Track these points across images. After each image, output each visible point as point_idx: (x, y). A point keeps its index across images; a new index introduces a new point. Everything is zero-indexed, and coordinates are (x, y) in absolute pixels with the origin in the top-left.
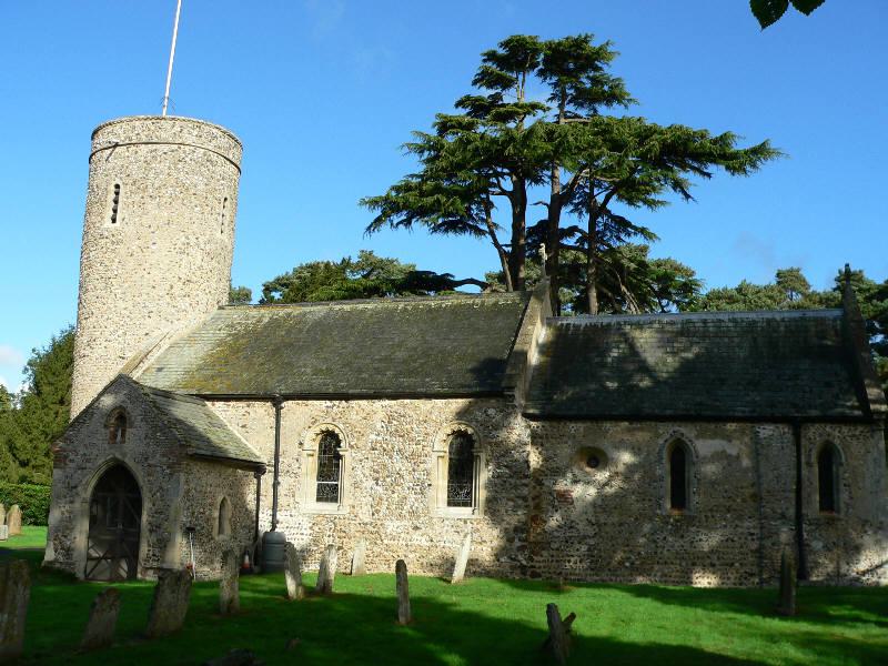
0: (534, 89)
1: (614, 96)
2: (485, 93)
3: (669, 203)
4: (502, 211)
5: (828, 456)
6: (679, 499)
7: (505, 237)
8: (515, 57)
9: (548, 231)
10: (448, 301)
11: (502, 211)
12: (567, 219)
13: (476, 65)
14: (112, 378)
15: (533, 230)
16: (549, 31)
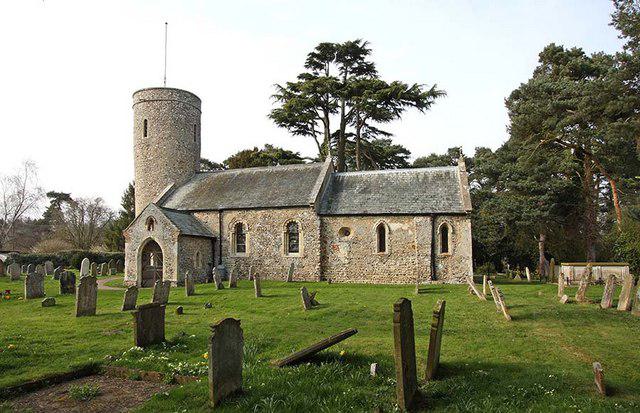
0: (334, 69)
1: (370, 69)
2: (310, 71)
3: (445, 94)
4: (320, 126)
5: (444, 230)
6: (382, 248)
7: (321, 139)
8: (326, 52)
9: (340, 134)
10: (300, 167)
11: (320, 126)
12: (350, 129)
13: (304, 58)
14: (494, 360)
15: (334, 135)
16: (340, 38)
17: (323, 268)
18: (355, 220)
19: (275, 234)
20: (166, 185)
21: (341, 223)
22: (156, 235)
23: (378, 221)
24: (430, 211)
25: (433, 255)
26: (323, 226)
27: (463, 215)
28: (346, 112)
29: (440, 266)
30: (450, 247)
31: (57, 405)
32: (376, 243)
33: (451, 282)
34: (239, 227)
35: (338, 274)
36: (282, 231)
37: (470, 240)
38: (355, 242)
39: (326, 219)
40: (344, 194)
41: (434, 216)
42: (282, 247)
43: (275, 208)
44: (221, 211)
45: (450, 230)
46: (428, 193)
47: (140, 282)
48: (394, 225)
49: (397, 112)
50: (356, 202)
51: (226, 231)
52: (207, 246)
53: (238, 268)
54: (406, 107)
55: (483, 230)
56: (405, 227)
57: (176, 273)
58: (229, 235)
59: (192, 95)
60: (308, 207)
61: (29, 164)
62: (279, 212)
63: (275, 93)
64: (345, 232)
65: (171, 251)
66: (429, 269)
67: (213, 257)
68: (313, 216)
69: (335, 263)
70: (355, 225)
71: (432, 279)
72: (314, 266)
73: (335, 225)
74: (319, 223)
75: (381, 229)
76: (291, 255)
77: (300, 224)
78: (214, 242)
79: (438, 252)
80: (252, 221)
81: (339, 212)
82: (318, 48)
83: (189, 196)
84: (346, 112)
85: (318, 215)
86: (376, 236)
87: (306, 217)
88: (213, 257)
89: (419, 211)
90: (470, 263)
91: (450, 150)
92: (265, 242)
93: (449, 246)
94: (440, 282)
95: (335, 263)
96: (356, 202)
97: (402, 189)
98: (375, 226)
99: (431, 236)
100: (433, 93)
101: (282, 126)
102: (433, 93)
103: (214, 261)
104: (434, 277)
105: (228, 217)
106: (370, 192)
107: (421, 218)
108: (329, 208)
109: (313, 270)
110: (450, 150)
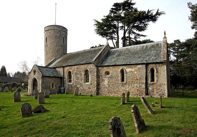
5: (152, 71)
6: (123, 80)
17: (98, 89)
18: (111, 68)
19: (81, 75)
20: (53, 59)
21: (106, 69)
22: (35, 77)
23: (121, 68)
24: (145, 62)
25: (146, 83)
26: (98, 71)
27: (162, 63)
28: (126, 29)
29: (150, 88)
30: (156, 79)
31: (78, 128)
32: (120, 78)
33: (155, 96)
34: (70, 73)
35: (104, 92)
36: (83, 73)
37: (166, 75)
38: (111, 77)
39: (100, 68)
40: (110, 57)
41: (147, 65)
42: (83, 80)
43: (80, 64)
44: (64, 67)
45: (155, 71)
46: (146, 54)
47: (32, 94)
48: (128, 70)
49: (146, 25)
50: (113, 60)
51: (65, 74)
52: (58, 81)
53: (69, 89)
54: (149, 23)
55: (182, 71)
56: (133, 70)
57: (41, 90)
58: (66, 76)
59: (62, 27)
60: (91, 63)
61: (38, 58)
62: (82, 66)
63: (95, 24)
64: (108, 73)
65: (39, 82)
66: (144, 90)
67: (61, 84)
68: (94, 67)
69: (103, 87)
70: (111, 70)
71: (146, 95)
72: (95, 88)
73: (103, 70)
74: (96, 70)
75: (122, 71)
76: (87, 83)
77: (89, 71)
78: (62, 79)
79: (149, 82)
80: (73, 69)
81: (105, 65)
82: (114, 6)
83: (58, 63)
84: (126, 29)
85: (96, 66)
86: (120, 75)
87: (91, 68)
88: (61, 84)
89: (140, 62)
90: (166, 87)
91: (175, 41)
92: (77, 78)
93: (155, 79)
94: (149, 96)
95: (103, 87)
96: (113, 60)
97: (135, 53)
98: (120, 70)
99: (84, 65)
100: (158, 14)
101: (103, 37)
102: (158, 14)
103: (61, 86)
104: (147, 94)
105: (66, 69)
106: (120, 56)
107: (140, 66)
108: (102, 63)
109: (94, 89)
110: (175, 41)
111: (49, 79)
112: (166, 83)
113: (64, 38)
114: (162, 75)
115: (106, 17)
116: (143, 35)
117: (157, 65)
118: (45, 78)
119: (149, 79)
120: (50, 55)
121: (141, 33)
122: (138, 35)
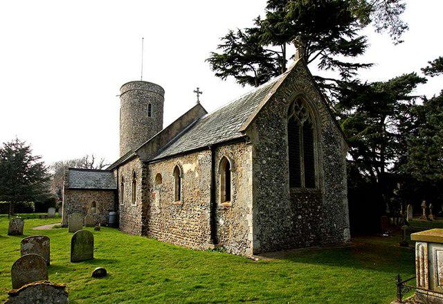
25: (214, 206)
29: (221, 222)
41: (214, 148)
75: (178, 172)
111: (84, 195)
112: (250, 206)
113: (150, 105)
114: (244, 181)
115: (227, 40)
116: (366, 63)
117: (235, 147)
118: (74, 193)
119: (220, 193)
120: (125, 143)
121: (359, 59)
122: (348, 65)
